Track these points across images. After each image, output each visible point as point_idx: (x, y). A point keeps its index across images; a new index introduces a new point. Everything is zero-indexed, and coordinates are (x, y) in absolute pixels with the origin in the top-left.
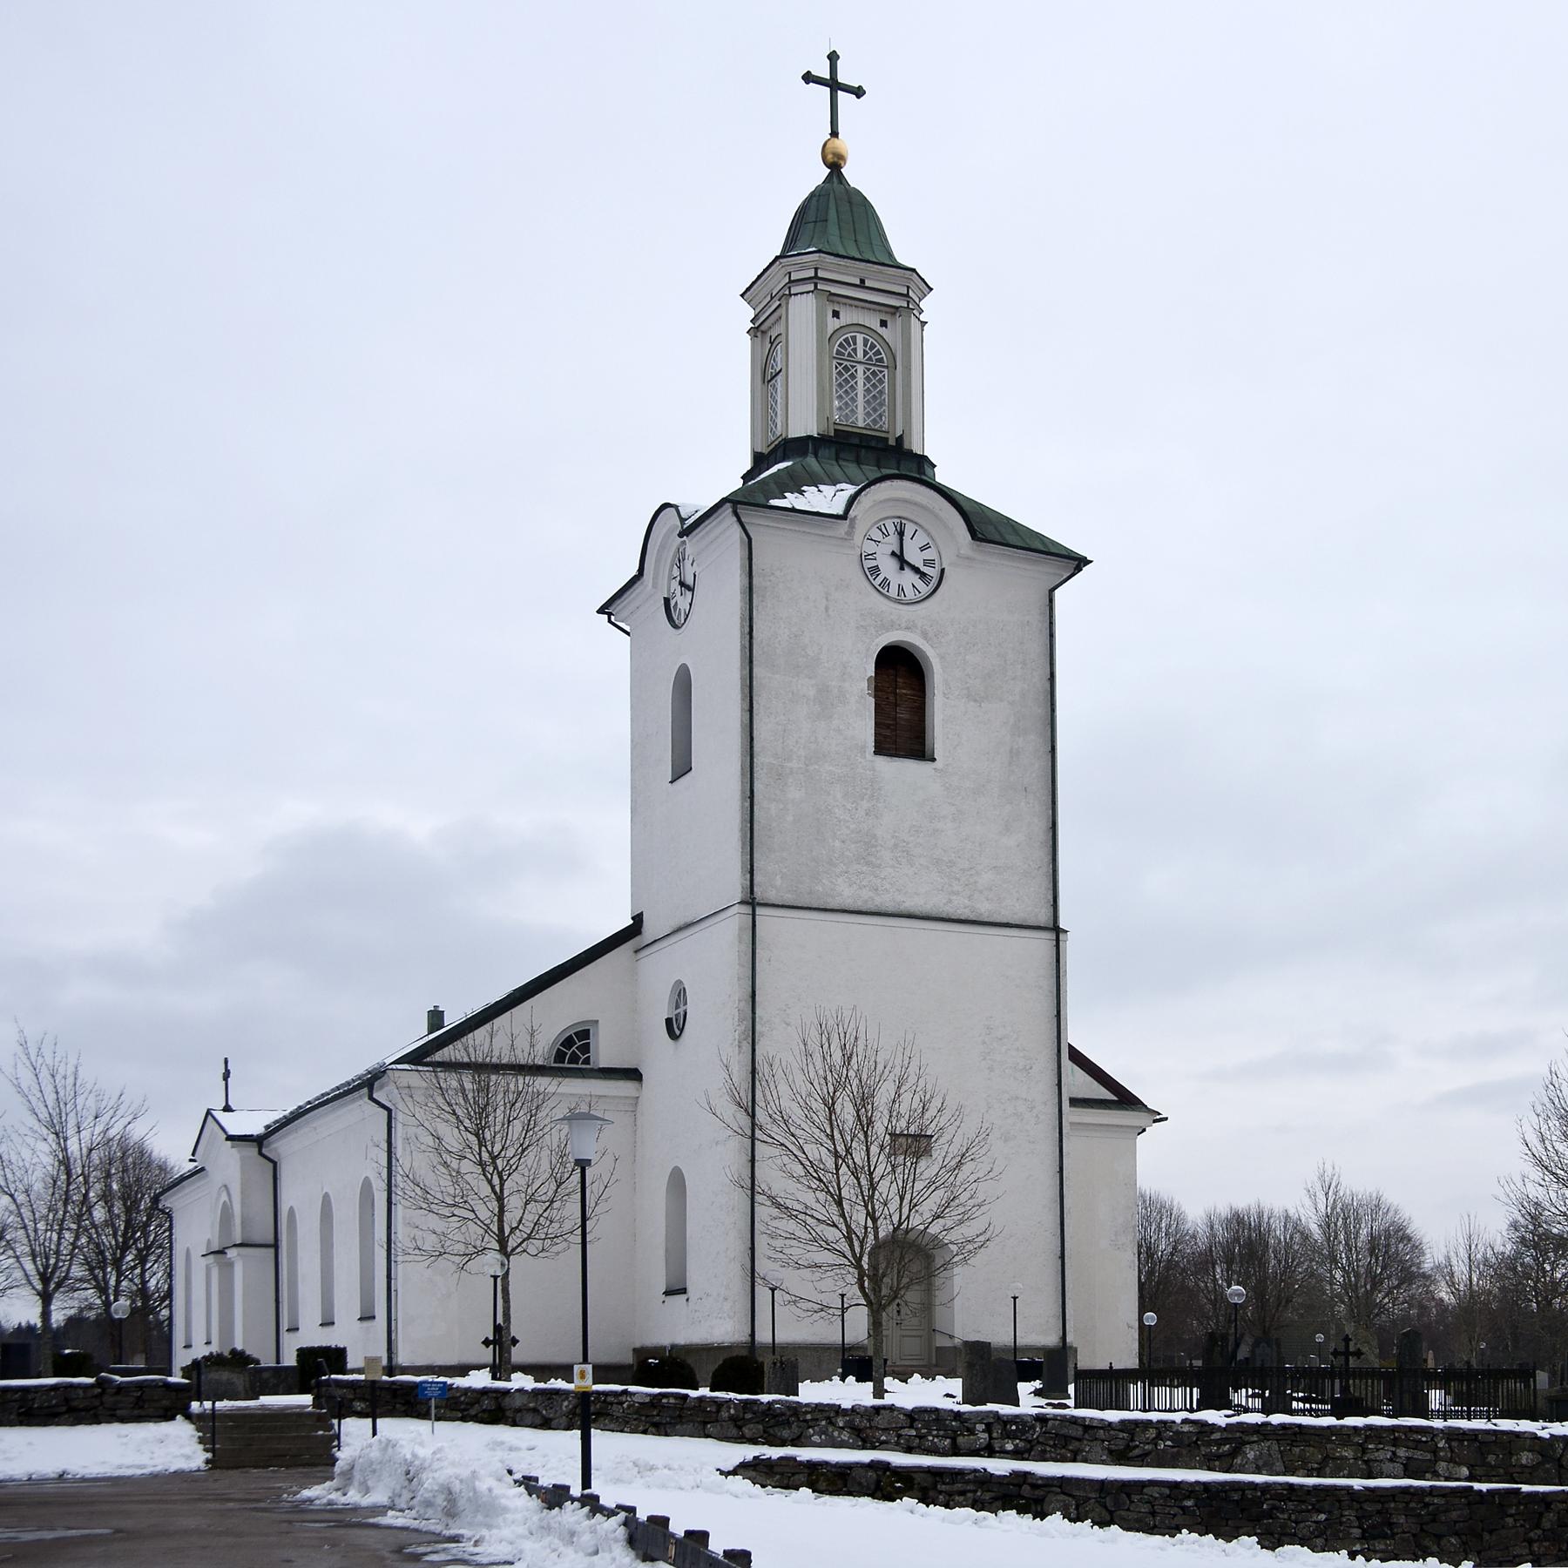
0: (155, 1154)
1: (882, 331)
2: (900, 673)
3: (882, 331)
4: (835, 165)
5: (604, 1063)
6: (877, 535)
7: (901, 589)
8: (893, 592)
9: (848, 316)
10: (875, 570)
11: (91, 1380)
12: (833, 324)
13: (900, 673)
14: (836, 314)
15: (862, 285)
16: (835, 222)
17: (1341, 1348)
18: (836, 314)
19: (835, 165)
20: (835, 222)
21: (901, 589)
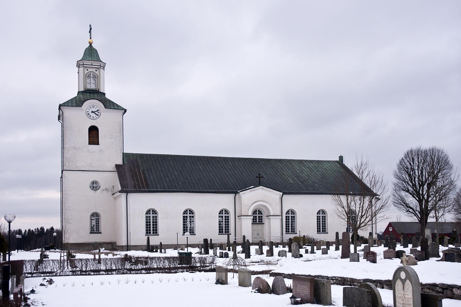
0: (450, 163)
1: (96, 72)
2: (93, 132)
3: (96, 72)
4: (91, 44)
5: (71, 241)
6: (89, 108)
7: (93, 117)
8: (92, 118)
9: (90, 70)
10: (89, 114)
11: (454, 247)
12: (86, 72)
13: (93, 132)
14: (87, 70)
15: (92, 65)
16: (91, 53)
17: (261, 176)
18: (87, 70)
19: (91, 44)
20: (91, 53)
21: (93, 117)
